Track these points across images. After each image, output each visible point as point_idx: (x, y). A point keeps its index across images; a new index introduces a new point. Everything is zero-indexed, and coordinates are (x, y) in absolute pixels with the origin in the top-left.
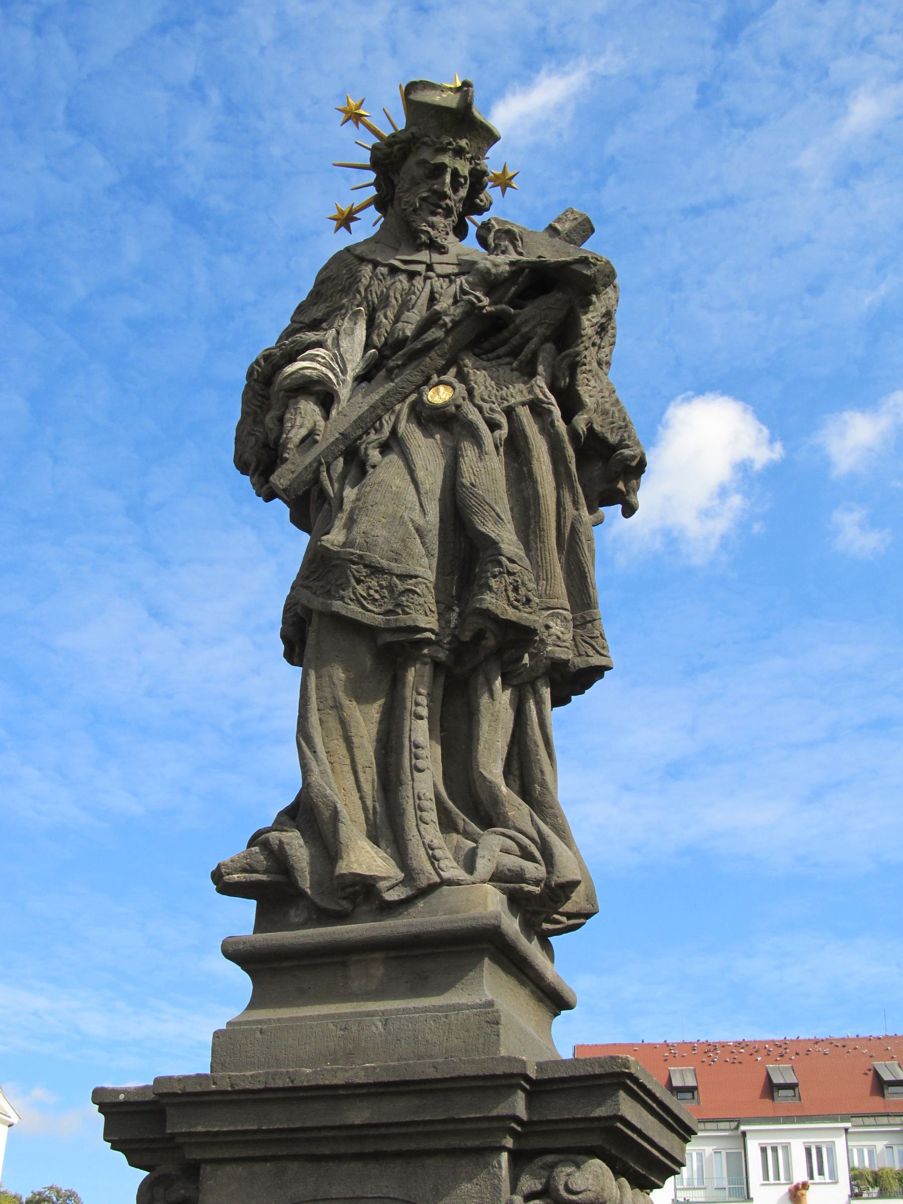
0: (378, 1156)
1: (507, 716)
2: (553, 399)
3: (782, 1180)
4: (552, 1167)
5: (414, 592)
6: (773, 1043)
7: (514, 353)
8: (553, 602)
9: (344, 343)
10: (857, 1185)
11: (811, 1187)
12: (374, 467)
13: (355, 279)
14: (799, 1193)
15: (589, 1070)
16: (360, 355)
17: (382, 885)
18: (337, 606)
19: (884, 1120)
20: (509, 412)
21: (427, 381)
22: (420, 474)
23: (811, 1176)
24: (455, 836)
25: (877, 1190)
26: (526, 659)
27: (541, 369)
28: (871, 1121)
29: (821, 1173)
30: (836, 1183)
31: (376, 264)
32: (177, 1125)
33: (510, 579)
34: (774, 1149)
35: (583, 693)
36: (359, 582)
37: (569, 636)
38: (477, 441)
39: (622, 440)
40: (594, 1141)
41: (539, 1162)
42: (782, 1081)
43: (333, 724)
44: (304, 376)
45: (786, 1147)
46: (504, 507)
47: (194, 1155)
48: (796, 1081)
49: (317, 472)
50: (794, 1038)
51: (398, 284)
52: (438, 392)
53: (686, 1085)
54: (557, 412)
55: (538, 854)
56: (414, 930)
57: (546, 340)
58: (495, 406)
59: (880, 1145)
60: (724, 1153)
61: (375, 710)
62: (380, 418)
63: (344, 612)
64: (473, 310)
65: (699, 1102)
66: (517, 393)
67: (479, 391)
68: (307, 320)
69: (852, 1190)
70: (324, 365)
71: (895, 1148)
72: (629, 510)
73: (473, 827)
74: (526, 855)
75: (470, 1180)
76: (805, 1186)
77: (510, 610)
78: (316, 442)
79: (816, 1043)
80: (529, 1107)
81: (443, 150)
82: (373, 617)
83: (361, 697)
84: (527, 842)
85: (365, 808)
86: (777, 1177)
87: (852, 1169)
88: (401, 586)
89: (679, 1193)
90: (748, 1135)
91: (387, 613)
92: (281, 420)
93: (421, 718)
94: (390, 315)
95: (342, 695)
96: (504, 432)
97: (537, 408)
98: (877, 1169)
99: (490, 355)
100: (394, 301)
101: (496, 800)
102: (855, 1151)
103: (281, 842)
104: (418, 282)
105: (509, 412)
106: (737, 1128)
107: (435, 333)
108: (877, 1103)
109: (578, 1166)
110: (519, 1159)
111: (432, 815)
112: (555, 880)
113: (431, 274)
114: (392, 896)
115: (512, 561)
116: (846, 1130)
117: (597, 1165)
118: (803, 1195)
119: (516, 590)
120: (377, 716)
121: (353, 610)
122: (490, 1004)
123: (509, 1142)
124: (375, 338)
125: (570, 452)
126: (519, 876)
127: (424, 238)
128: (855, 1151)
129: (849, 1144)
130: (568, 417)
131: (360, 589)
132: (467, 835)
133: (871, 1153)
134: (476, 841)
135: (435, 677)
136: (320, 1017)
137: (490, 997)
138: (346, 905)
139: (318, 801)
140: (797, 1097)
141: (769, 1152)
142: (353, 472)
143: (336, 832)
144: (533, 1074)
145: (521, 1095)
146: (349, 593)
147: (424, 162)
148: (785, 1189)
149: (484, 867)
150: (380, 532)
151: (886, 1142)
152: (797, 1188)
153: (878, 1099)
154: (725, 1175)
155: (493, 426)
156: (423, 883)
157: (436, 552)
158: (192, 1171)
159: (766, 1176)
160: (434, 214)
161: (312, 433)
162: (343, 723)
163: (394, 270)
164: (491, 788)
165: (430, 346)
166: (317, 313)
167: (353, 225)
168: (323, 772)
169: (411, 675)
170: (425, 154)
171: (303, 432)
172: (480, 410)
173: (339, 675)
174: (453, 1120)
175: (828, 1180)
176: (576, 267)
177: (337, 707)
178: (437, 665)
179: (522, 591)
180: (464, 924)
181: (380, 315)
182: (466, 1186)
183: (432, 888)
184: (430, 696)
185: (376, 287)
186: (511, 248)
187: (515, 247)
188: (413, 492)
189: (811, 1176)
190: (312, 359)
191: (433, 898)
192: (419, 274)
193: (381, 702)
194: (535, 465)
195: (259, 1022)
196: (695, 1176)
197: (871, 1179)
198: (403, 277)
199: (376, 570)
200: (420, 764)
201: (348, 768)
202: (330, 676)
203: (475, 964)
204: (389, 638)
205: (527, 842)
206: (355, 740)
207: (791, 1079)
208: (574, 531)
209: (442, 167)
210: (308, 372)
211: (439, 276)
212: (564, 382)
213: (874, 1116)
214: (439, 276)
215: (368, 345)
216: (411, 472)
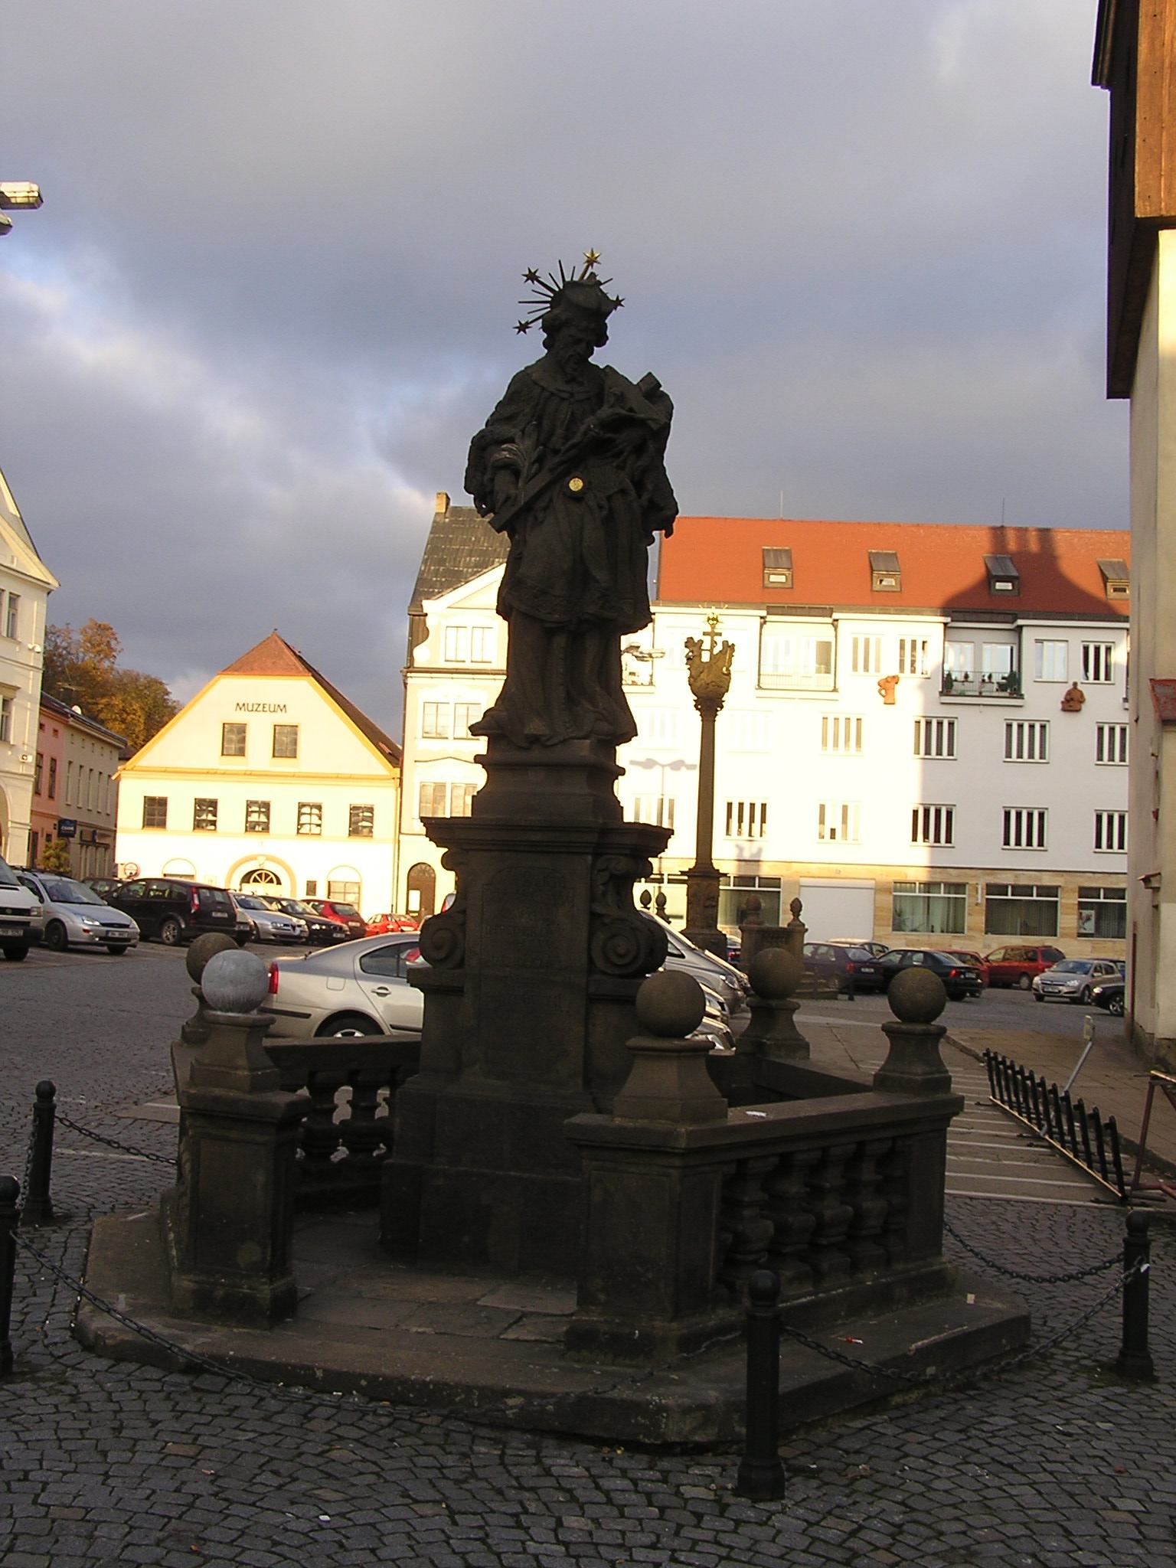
76: (895, 679)
96: (605, 512)
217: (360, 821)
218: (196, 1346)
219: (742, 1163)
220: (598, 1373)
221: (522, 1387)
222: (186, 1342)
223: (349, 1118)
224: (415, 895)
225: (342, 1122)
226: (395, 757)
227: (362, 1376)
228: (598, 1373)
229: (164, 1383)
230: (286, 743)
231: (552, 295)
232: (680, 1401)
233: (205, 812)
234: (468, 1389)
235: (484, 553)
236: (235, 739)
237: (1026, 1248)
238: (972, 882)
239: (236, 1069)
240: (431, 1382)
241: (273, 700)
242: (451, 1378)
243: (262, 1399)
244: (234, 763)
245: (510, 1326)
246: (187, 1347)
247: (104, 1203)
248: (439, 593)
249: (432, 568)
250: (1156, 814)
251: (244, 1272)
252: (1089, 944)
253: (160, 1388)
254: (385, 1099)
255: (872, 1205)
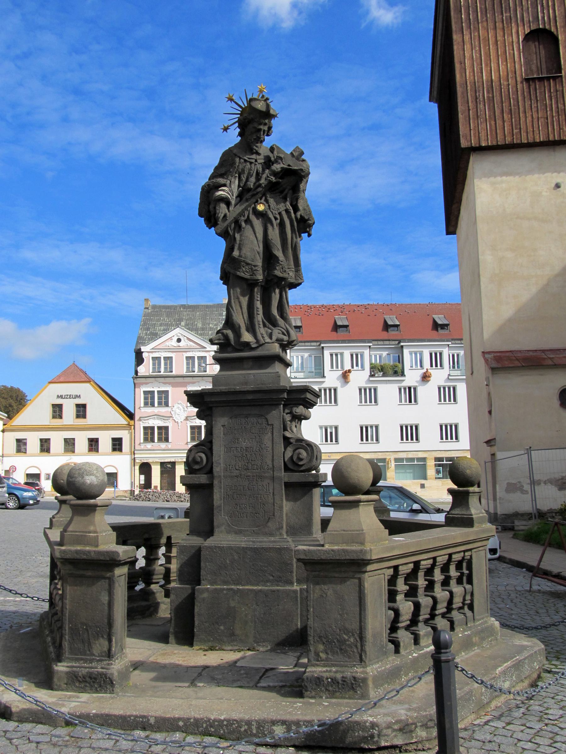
0: (254, 405)
1: (278, 296)
2: (291, 208)
3: (340, 369)
4: (292, 407)
5: (257, 270)
6: (338, 306)
7: (281, 192)
8: (290, 267)
9: (232, 186)
10: (373, 371)
11: (352, 372)
12: (243, 228)
13: (234, 163)
14: (347, 374)
15: (300, 388)
16: (237, 189)
17: (251, 343)
18: (238, 273)
19: (387, 342)
20: (280, 214)
21: (257, 201)
22: (257, 235)
23: (353, 367)
24: (266, 328)
25: (382, 373)
26: (283, 283)
27: (288, 199)
28: (381, 343)
29: (357, 365)
30: (364, 370)
31: (240, 158)
32: (207, 399)
33: (281, 266)
34: (336, 355)
35: (296, 288)
36: (243, 267)
37: (294, 276)
38: (272, 225)
39: (309, 218)
40: (301, 402)
41: (289, 406)
42: (341, 324)
43: (237, 302)
44: (222, 197)
45: (342, 354)
46: (279, 246)
47: (211, 405)
48: (348, 324)
49: (227, 228)
50: (348, 304)
51: (247, 166)
52: (260, 206)
53: (297, 325)
54: (292, 211)
55: (286, 333)
56: (260, 355)
57: (290, 189)
58: (276, 212)
59: (385, 354)
60: (313, 356)
61: (247, 298)
62: (244, 212)
63: (240, 275)
64: (270, 182)
65: (302, 333)
66: (282, 207)
67: (272, 206)
68: (219, 173)
69: (371, 373)
70: (227, 193)
71: (391, 355)
72: (309, 235)
73: (270, 326)
74: (283, 334)
75: (274, 410)
76: (349, 371)
77: (281, 274)
78: (227, 219)
79: (359, 306)
80: (287, 395)
81: (261, 124)
82: (247, 276)
83: (244, 295)
84: (283, 330)
85: (245, 323)
86: (337, 367)
87: (371, 364)
88: (254, 268)
89: (292, 374)
90: (324, 348)
91: (251, 275)
92: (215, 208)
93: (258, 301)
94: (245, 177)
95: (239, 296)
96: (278, 221)
97: (287, 211)
98: (382, 364)
99: (274, 192)
100: (246, 172)
101: (276, 320)
102: (373, 356)
103: (227, 334)
104: (253, 165)
105: (280, 214)
106: (320, 345)
107: (260, 189)
108: (385, 335)
109: (297, 407)
110: (285, 406)
111: (261, 323)
112: (291, 340)
113: (256, 163)
114: (253, 346)
115: (282, 262)
116: (370, 347)
117: (301, 407)
118: (348, 375)
119: (282, 269)
120: (247, 299)
121: (242, 275)
122: (278, 372)
123: (283, 403)
124: (241, 184)
125: (295, 224)
126: (282, 340)
127: (254, 151)
128: (373, 356)
129: (371, 353)
130: (295, 212)
131: (244, 269)
132: (269, 328)
133: (380, 357)
134: (272, 330)
135: (261, 288)
136: (238, 374)
137: (278, 371)
138: (242, 348)
139: (235, 323)
140: (348, 332)
141: (334, 356)
142: (237, 228)
143: (240, 331)
144: (288, 389)
145: (286, 394)
146: (241, 270)
147: (255, 128)
148: (341, 372)
149: (274, 338)
150: (248, 254)
151: (387, 352)
152: (346, 372)
153: (385, 333)
154: (313, 366)
155: (276, 219)
156: (261, 343)
157: (262, 258)
158: (211, 409)
159: (332, 367)
160: (257, 143)
161: (225, 216)
162: (240, 302)
163: (245, 161)
164: (275, 316)
165: (258, 193)
166: (223, 170)
167: (228, 130)
168: (236, 316)
169: (256, 290)
170: (256, 125)
171: (223, 215)
172: (272, 213)
173: (238, 290)
174: (271, 398)
175: (360, 369)
176: (299, 171)
177: (238, 298)
178: (262, 286)
179: (284, 269)
180: (272, 354)
181: (242, 176)
182: (274, 412)
183: (263, 344)
184: (260, 295)
185: (241, 167)
186: (281, 162)
187: (282, 162)
188: (256, 241)
189: (353, 367)
190: (223, 190)
191: (263, 347)
192: (253, 163)
193: (248, 296)
194: (286, 229)
195: (223, 375)
196: (300, 366)
197: (380, 368)
198: (248, 164)
199: (248, 264)
200: (259, 313)
201: (241, 313)
202: (236, 291)
203: (274, 362)
204: (251, 282)
205: (283, 330)
206: (243, 306)
207: (346, 323)
208: (296, 246)
209: (260, 130)
210: (223, 195)
211: (259, 164)
212: (294, 203)
213: (383, 340)
214: (259, 164)
215: (239, 186)
216: (255, 234)
217: (117, 444)
218: (70, 708)
219: (396, 568)
220: (327, 704)
221: (284, 718)
222: (63, 705)
223: (144, 565)
224: (143, 477)
225: (141, 568)
226: (131, 416)
227: (179, 719)
228: (327, 704)
229: (52, 735)
230: (81, 411)
231: (241, 110)
232: (385, 719)
233: (45, 447)
234: (249, 723)
235: (167, 325)
236: (57, 411)
237: (498, 613)
238: (388, 457)
239: (90, 532)
240: (225, 720)
241: (74, 393)
242: (235, 716)
243: (117, 741)
244: (57, 422)
245: (261, 678)
246: (63, 710)
247: (5, 624)
248: (147, 342)
249: (144, 332)
250: (490, 412)
251: (98, 658)
252: (441, 482)
253: (49, 740)
254: (163, 554)
255: (457, 590)
